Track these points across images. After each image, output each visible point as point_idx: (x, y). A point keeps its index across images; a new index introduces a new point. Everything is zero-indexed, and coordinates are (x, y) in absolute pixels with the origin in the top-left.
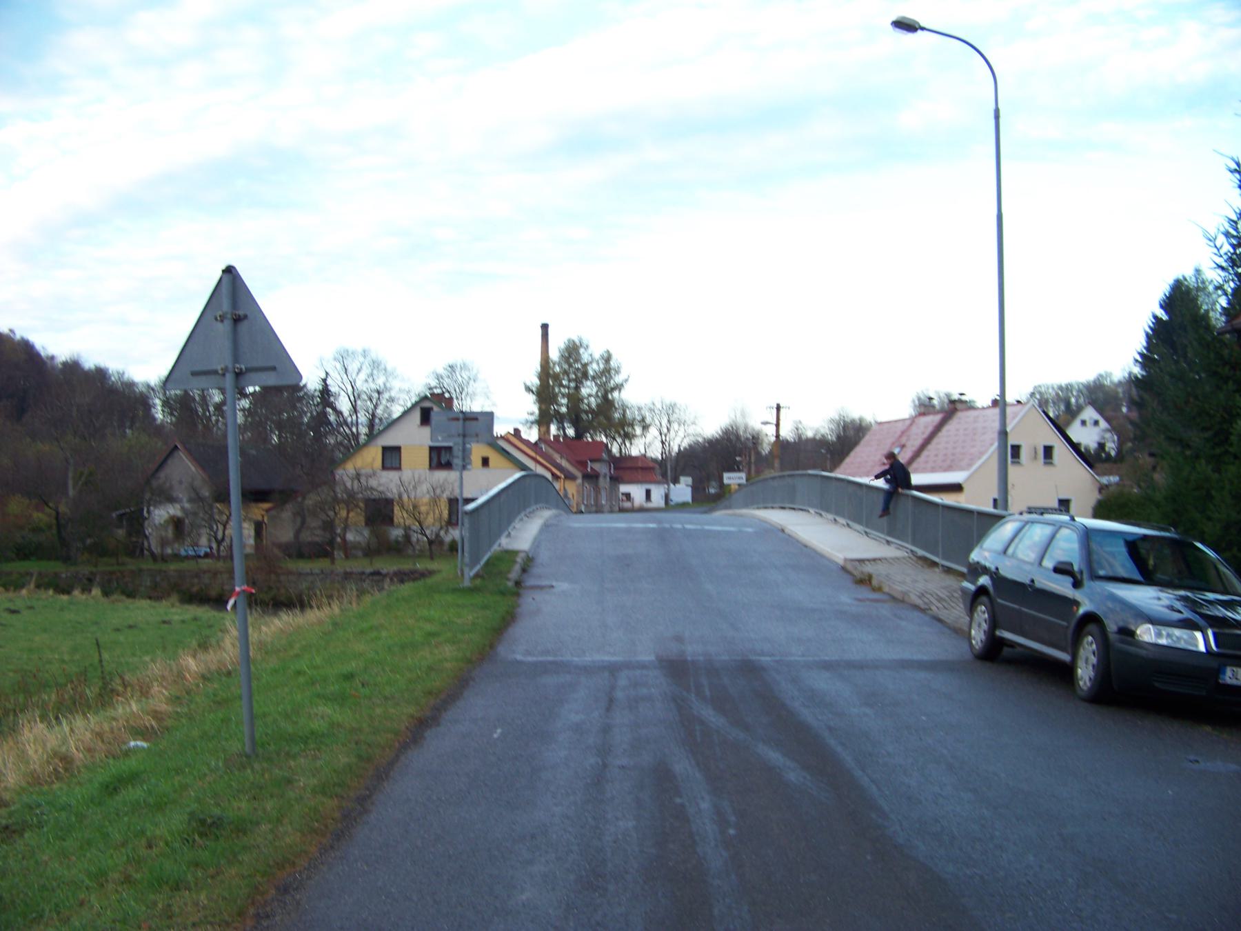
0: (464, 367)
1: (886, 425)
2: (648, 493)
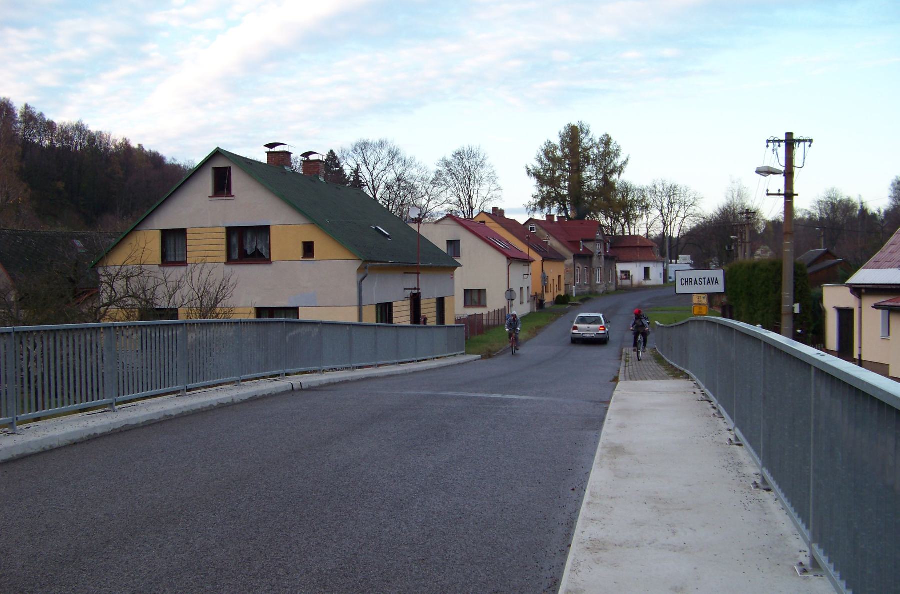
0: (472, 154)
2: (647, 271)
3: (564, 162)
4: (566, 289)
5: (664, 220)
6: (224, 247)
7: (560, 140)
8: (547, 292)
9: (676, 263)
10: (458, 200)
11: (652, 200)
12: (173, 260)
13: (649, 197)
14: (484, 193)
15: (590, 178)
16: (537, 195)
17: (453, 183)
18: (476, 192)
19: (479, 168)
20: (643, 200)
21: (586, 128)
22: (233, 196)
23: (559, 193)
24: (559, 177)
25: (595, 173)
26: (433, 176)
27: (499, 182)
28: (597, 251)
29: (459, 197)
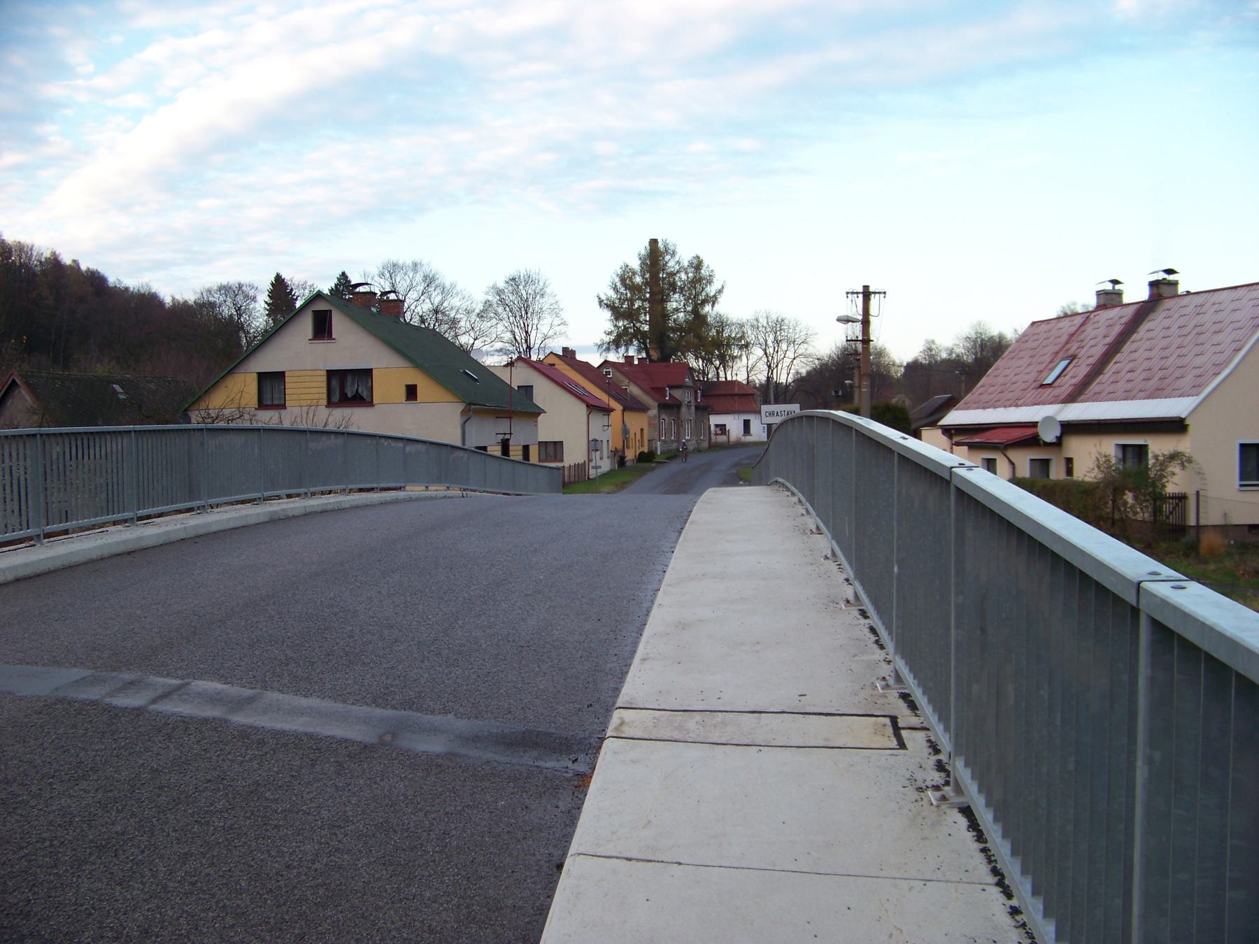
0: (529, 280)
1: (1043, 326)
2: (747, 424)
3: (645, 290)
4: (649, 445)
5: (768, 361)
6: (325, 390)
7: (639, 262)
8: (628, 447)
10: (511, 336)
11: (753, 336)
12: (269, 402)
13: (750, 332)
14: (544, 328)
15: (677, 310)
16: (610, 330)
17: (506, 316)
18: (535, 326)
19: (538, 297)
20: (742, 337)
21: (672, 248)
22: (334, 339)
23: (638, 329)
24: (637, 308)
25: (682, 304)
26: (478, 309)
27: (563, 314)
28: (686, 399)
29: (513, 333)
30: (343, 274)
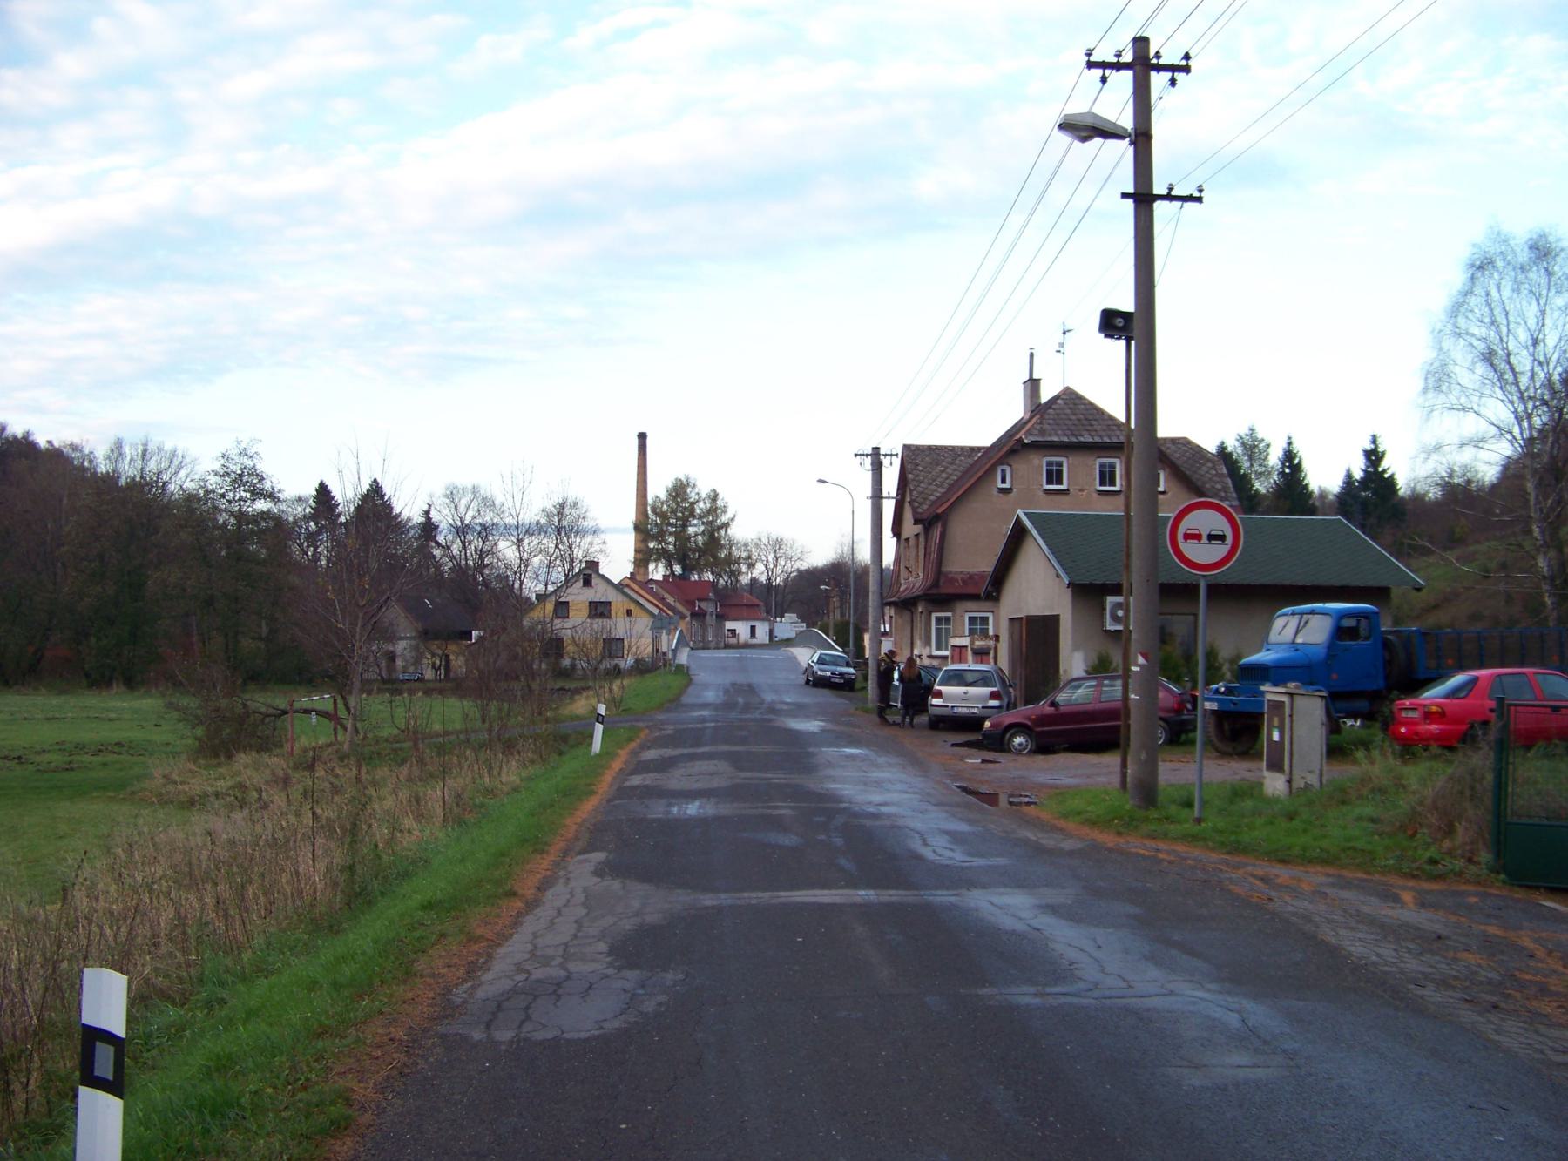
2: (753, 629)
9: (781, 621)
30: (375, 481)
